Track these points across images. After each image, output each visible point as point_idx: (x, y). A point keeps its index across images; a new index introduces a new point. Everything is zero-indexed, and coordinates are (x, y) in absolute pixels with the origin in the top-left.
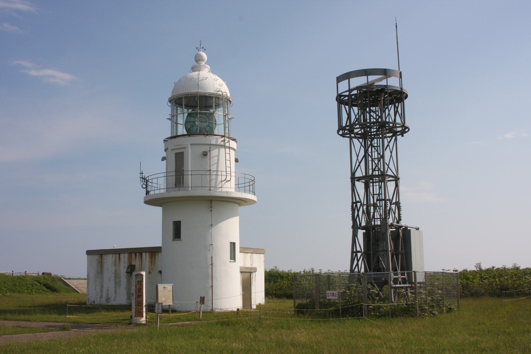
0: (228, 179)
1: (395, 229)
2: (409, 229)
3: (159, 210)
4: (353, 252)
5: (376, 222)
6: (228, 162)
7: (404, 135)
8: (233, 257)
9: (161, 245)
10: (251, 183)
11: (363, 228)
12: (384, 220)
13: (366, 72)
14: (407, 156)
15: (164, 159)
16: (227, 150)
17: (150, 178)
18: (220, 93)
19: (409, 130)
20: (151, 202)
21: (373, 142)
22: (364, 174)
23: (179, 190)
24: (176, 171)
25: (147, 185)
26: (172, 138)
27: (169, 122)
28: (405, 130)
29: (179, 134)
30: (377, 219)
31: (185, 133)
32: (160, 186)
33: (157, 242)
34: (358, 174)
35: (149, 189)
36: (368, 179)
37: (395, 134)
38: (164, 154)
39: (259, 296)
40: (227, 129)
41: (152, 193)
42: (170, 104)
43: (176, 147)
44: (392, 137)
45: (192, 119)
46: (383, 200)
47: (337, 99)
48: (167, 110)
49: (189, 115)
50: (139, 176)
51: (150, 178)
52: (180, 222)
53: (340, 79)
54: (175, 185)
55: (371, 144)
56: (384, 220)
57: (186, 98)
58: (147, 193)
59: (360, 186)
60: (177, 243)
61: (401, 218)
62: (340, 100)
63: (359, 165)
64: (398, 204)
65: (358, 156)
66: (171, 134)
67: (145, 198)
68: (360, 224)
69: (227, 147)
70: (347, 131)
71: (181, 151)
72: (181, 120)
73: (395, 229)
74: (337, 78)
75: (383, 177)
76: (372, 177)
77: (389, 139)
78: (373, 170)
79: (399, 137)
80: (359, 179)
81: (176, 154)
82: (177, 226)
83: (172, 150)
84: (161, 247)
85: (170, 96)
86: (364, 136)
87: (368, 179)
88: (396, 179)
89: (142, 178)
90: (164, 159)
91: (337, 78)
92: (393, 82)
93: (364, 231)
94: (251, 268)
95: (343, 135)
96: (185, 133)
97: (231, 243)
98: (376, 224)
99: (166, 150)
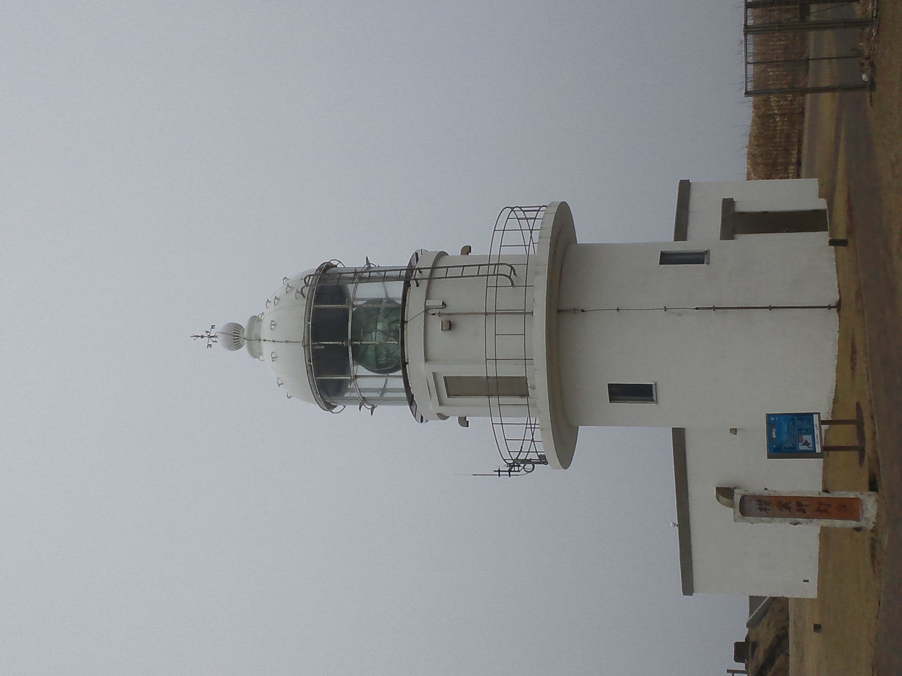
0: (506, 270)
6: (468, 271)
8: (699, 258)
10: (520, 214)
15: (464, 422)
16: (440, 273)
17: (507, 457)
18: (306, 291)
23: (533, 388)
24: (489, 396)
25: (526, 461)
26: (411, 401)
31: (400, 373)
32: (521, 427)
35: (535, 457)
38: (454, 420)
39: (798, 194)
41: (540, 447)
45: (370, 353)
49: (360, 358)
50: (505, 478)
51: (507, 457)
54: (522, 396)
57: (318, 372)
58: (543, 460)
60: (662, 393)
66: (404, 404)
69: (431, 273)
82: (622, 393)
89: (510, 471)
90: (464, 422)
96: (400, 373)
99: (443, 417)
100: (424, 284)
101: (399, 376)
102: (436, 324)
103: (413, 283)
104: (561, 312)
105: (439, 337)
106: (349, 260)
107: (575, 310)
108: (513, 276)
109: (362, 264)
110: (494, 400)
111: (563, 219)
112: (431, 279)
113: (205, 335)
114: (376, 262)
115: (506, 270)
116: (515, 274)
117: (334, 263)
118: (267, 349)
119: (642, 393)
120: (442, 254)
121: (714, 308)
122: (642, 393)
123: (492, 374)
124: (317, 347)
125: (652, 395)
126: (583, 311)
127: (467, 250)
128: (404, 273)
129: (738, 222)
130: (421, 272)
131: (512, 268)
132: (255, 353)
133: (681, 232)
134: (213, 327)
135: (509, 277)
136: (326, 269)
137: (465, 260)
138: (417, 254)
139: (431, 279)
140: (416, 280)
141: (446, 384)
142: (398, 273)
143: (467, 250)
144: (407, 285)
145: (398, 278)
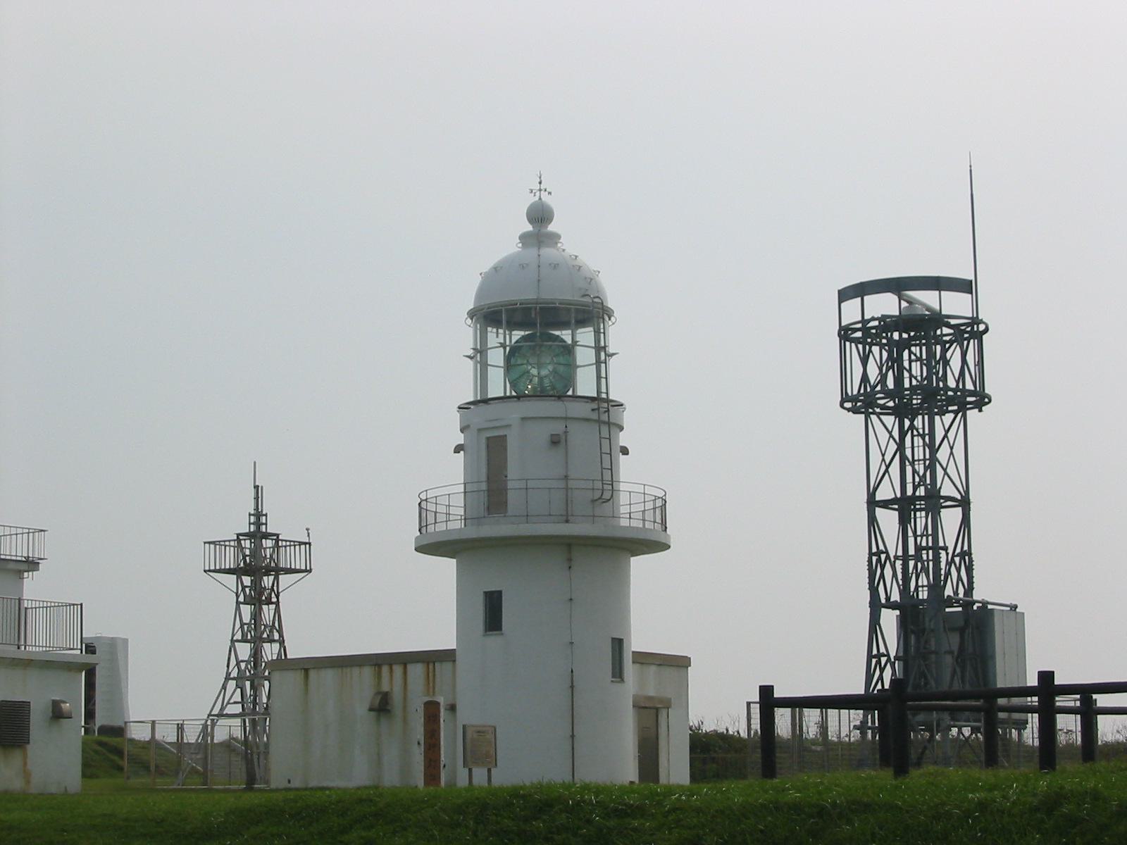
1: (960, 609)
2: (990, 607)
3: (447, 567)
4: (870, 656)
5: (920, 593)
6: (606, 458)
7: (984, 408)
8: (618, 673)
9: (455, 648)
10: (659, 503)
11: (893, 606)
12: (936, 587)
13: (897, 286)
14: (989, 452)
15: (458, 449)
16: (605, 429)
19: (990, 401)
20: (431, 547)
21: (915, 423)
22: (899, 495)
27: (471, 362)
28: (982, 400)
29: (490, 396)
30: (923, 586)
33: (445, 639)
34: (884, 493)
36: (904, 506)
37: (963, 408)
38: (460, 439)
39: (676, 768)
40: (603, 381)
41: (431, 529)
42: (469, 321)
43: (491, 425)
44: (956, 412)
46: (930, 548)
47: (839, 334)
48: (466, 336)
52: (500, 593)
53: (844, 295)
55: (912, 427)
56: (936, 587)
59: (888, 520)
61: (975, 585)
62: (845, 334)
63: (887, 471)
64: (966, 555)
65: (883, 455)
66: (474, 305)
67: (417, 538)
68: (888, 598)
69: (604, 423)
70: (862, 403)
71: (501, 433)
72: (496, 357)
73: (960, 609)
74: (839, 291)
75: (934, 502)
76: (914, 498)
77: (951, 416)
78: (915, 488)
79: (972, 414)
80: (885, 504)
81: (488, 439)
83: (479, 430)
84: (454, 650)
85: (472, 307)
86: (903, 411)
87: (904, 506)
88: (964, 503)
90: (458, 449)
91: (839, 291)
92: (955, 305)
93: (897, 612)
94: (661, 700)
95: (855, 410)
97: (613, 639)
98: (920, 597)
100: (594, 416)
101: (505, 392)
102: (558, 428)
103: (594, 405)
104: (570, 547)
105: (542, 432)
106: (615, 334)
107: (570, 560)
108: (601, 501)
109: (611, 350)
110: (484, 486)
111: (653, 545)
112: (599, 422)
113: (543, 187)
114: (612, 362)
115: (607, 495)
116: (604, 502)
117: (612, 318)
118: (533, 252)
119: (493, 621)
120: (621, 429)
121: (572, 687)
122: (493, 621)
123: (510, 485)
124: (533, 313)
125: (490, 630)
126: (570, 567)
127: (625, 451)
128: (604, 396)
129: (651, 713)
130: (605, 412)
131: (610, 500)
132: (525, 238)
133: (643, 659)
134: (550, 193)
135: (600, 498)
136: (608, 313)
137: (616, 450)
138: (622, 405)
139: (599, 422)
140: (598, 409)
141: (499, 437)
142: (604, 390)
143: (625, 451)
144: (592, 399)
145: (599, 392)
